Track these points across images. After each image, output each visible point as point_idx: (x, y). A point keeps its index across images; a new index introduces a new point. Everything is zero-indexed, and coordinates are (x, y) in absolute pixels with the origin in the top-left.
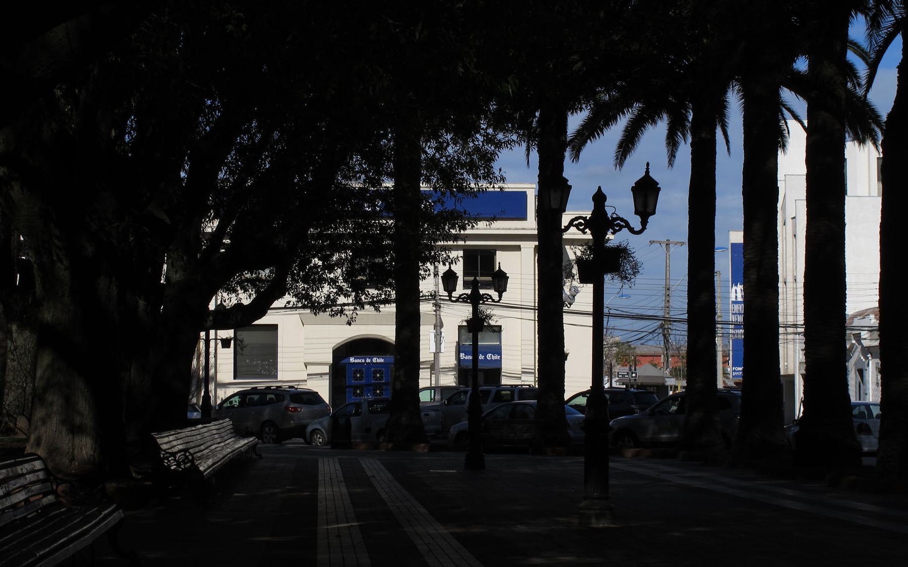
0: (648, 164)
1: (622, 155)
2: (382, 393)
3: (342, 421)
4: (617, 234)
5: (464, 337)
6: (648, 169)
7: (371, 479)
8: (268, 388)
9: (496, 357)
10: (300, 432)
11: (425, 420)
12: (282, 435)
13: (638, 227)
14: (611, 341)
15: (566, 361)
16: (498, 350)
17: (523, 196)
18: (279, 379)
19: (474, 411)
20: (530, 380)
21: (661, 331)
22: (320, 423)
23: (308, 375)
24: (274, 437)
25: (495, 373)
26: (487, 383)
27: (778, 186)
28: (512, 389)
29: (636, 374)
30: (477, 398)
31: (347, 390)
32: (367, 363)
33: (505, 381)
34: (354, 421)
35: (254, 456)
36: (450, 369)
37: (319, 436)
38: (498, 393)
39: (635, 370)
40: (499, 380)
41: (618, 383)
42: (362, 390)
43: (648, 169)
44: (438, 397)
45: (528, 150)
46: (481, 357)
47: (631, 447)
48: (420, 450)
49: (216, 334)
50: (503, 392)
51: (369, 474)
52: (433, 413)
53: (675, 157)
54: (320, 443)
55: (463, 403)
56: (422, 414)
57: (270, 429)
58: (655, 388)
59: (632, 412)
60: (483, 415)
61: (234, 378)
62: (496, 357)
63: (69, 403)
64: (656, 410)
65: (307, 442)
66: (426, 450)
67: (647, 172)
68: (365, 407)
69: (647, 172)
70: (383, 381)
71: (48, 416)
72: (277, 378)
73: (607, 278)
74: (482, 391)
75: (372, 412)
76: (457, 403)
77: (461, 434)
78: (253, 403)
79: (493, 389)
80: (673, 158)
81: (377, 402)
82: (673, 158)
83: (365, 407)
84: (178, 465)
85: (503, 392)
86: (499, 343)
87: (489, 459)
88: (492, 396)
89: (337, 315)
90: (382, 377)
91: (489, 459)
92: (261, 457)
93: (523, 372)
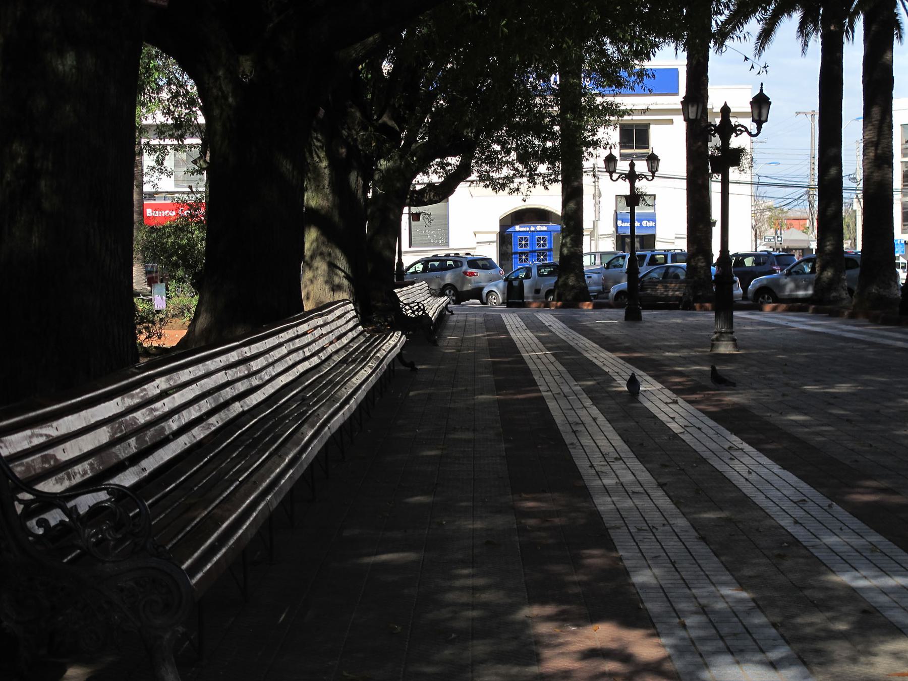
0: (762, 84)
1: (761, 46)
2: (546, 259)
3: (515, 283)
4: (739, 137)
5: (620, 205)
6: (762, 88)
7: (549, 327)
8: (448, 255)
9: (651, 224)
10: (477, 293)
11: (588, 281)
12: (460, 297)
13: (754, 132)
14: (763, 206)
15: (713, 228)
16: (652, 218)
17: (676, 71)
18: (450, 248)
19: (632, 272)
20: (682, 245)
21: (806, 197)
22: (496, 285)
23: (478, 243)
24: (454, 298)
25: (649, 240)
26: (643, 247)
27: (894, 75)
28: (666, 253)
29: (781, 237)
30: (635, 262)
31: (513, 256)
32: (531, 231)
33: (659, 246)
34: (526, 283)
35: (447, 313)
36: (609, 236)
37: (494, 297)
38: (653, 257)
39: (781, 234)
40: (653, 245)
41: (766, 247)
42: (527, 256)
43: (762, 88)
44: (598, 262)
45: (676, 49)
46: (637, 224)
47: (770, 303)
48: (585, 308)
49: (409, 210)
50: (657, 256)
51: (547, 324)
52: (595, 276)
53: (807, 46)
54: (495, 303)
55: (621, 266)
56: (586, 276)
57: (450, 292)
58: (800, 251)
59: (774, 272)
60: (640, 276)
61: (410, 247)
62: (651, 224)
63: (332, 266)
64: (792, 271)
65: (483, 303)
66: (590, 308)
67: (761, 90)
68: (534, 271)
69: (761, 90)
70: (547, 248)
71: (315, 277)
72: (448, 246)
73: (731, 169)
74: (639, 256)
75: (540, 275)
76: (615, 267)
77: (620, 293)
78: (434, 269)
79: (648, 253)
80: (806, 47)
81: (544, 266)
82: (806, 47)
83: (534, 271)
84: (413, 312)
85: (657, 256)
86: (653, 211)
87: (645, 314)
88: (647, 260)
89: (514, 192)
90: (545, 244)
91: (645, 314)
92: (453, 314)
93: (676, 238)
